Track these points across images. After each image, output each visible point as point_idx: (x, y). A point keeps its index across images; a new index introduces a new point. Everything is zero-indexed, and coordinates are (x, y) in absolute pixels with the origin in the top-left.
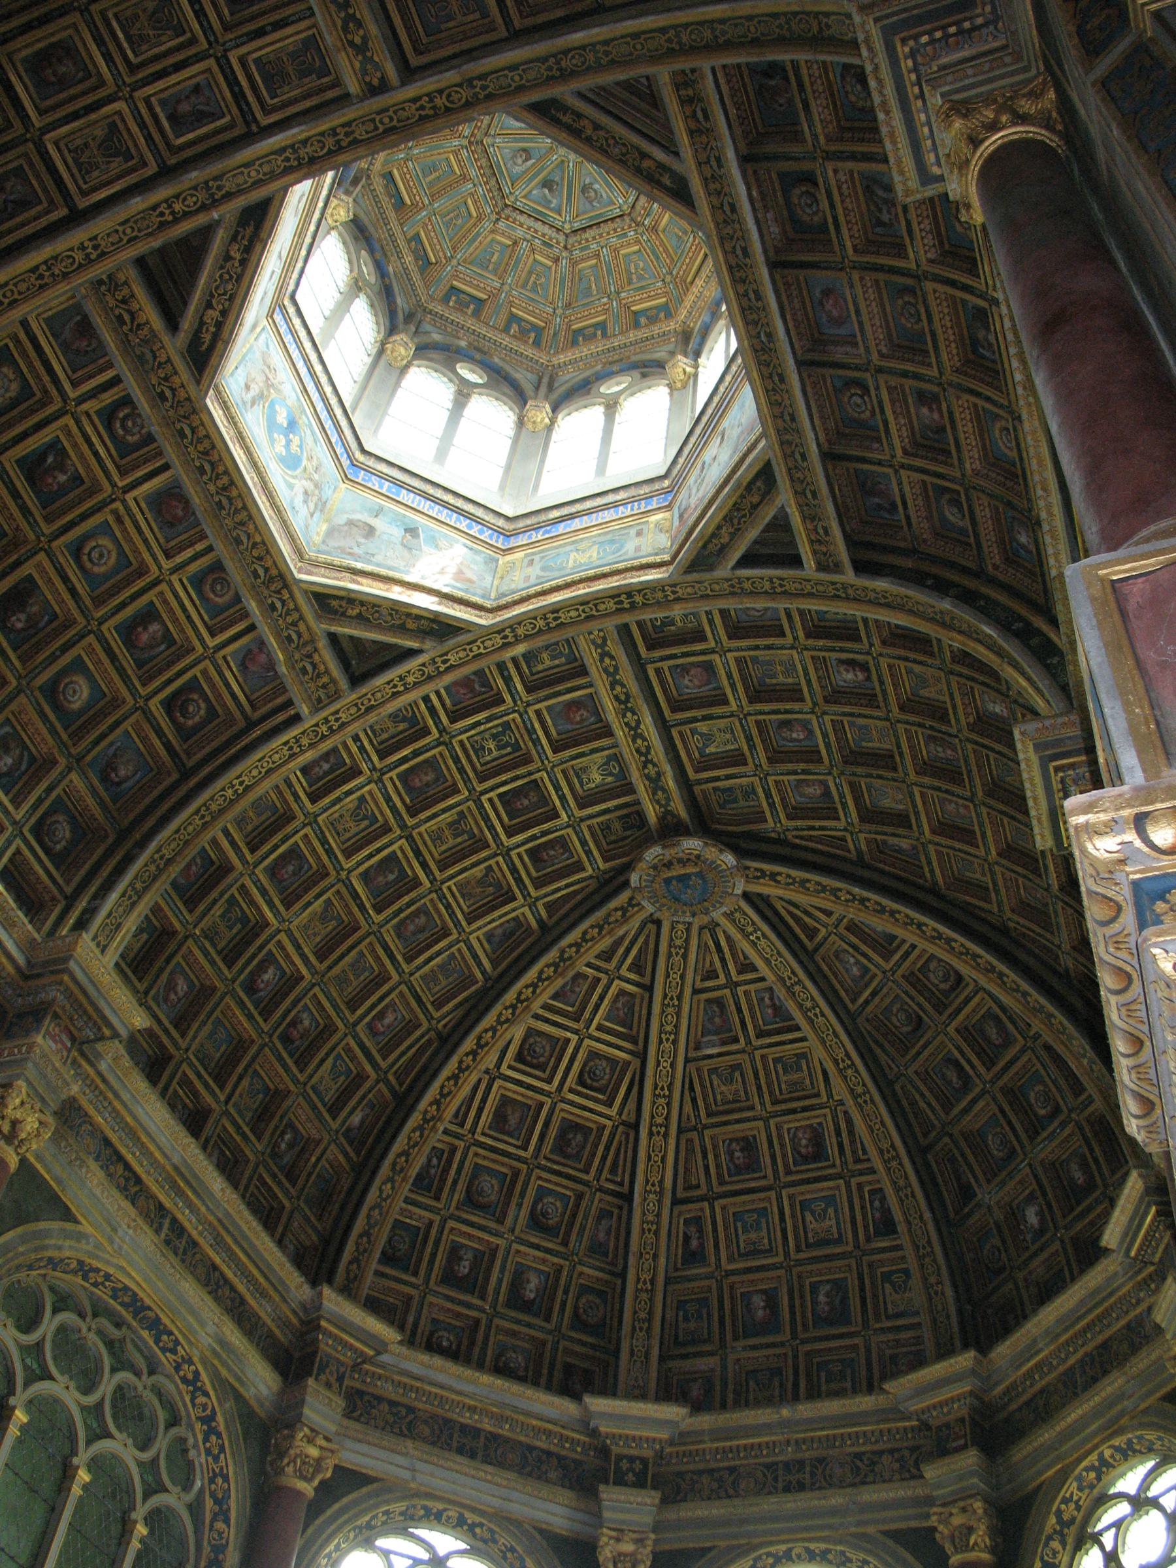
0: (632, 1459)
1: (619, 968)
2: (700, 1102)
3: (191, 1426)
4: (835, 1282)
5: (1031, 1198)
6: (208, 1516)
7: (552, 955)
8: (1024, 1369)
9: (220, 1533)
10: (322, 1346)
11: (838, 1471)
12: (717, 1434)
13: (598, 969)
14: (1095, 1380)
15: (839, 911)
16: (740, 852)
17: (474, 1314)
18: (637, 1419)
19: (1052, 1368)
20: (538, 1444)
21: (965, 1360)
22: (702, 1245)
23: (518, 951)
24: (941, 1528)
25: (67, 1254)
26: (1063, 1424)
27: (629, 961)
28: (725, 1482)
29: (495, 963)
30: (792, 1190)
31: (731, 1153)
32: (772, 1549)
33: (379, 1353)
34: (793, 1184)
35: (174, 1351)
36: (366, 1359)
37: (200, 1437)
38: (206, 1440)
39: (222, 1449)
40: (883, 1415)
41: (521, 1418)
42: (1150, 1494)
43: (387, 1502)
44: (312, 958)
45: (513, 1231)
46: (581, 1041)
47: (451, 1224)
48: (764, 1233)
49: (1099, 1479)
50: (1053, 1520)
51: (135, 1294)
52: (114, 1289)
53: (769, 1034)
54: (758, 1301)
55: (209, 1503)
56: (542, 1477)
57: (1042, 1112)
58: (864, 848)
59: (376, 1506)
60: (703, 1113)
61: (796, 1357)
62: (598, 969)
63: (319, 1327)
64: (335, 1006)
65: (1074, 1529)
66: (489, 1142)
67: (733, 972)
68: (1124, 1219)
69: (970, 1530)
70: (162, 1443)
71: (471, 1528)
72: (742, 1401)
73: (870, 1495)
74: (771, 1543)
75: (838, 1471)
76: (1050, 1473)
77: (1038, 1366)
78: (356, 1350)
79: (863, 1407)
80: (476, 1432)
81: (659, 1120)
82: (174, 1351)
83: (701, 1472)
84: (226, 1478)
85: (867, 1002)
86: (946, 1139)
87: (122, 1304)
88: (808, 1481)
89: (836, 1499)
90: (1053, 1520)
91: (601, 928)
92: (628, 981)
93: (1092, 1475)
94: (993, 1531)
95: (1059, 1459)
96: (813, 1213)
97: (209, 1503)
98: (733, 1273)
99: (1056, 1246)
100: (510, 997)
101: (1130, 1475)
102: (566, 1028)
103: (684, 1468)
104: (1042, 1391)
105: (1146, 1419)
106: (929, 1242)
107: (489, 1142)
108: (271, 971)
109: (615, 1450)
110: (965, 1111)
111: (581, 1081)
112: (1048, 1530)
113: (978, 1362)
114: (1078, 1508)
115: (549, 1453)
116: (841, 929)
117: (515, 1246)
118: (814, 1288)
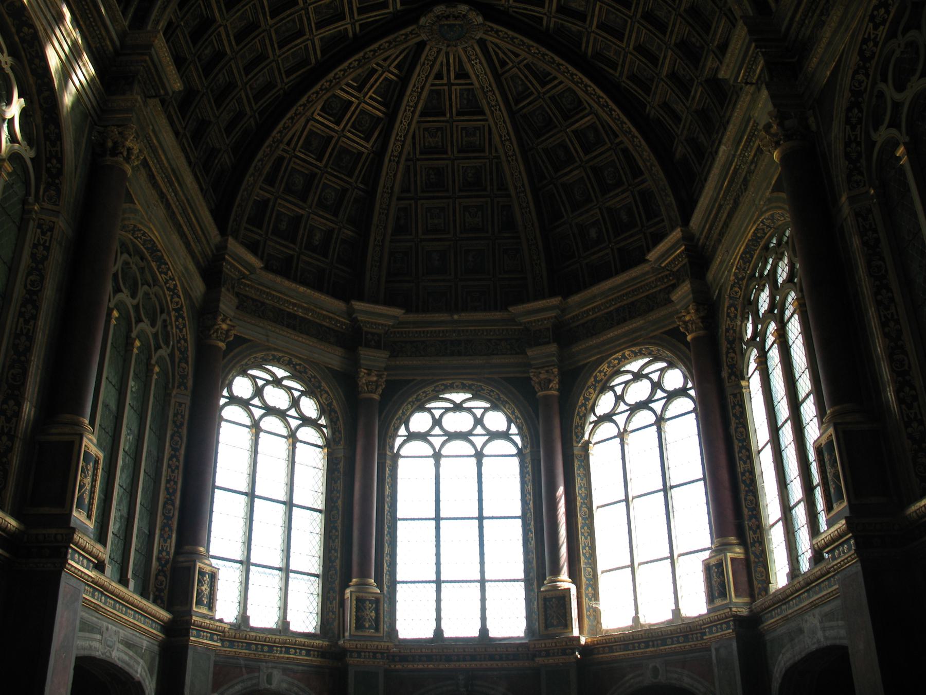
1: (389, 66)
3: (169, 314)
6: (177, 360)
9: (184, 369)
14: (625, 320)
15: (523, 54)
16: (486, 18)
18: (376, 314)
20: (324, 323)
21: (555, 301)
24: (534, 379)
26: (605, 337)
27: (396, 62)
32: (445, 382)
33: (251, 273)
35: (166, 274)
36: (244, 276)
37: (173, 319)
38: (177, 320)
39: (185, 326)
42: (644, 372)
45: (310, 207)
46: (359, 104)
47: (279, 201)
49: (619, 363)
50: (592, 379)
55: (177, 353)
58: (552, 25)
59: (250, 355)
63: (224, 259)
65: (601, 384)
66: (303, 156)
68: (664, 249)
69: (550, 381)
71: (294, 366)
73: (496, 360)
76: (594, 358)
77: (593, 308)
78: (239, 271)
80: (295, 316)
81: (395, 153)
82: (166, 274)
84: (186, 341)
85: (524, 107)
90: (592, 379)
92: (392, 73)
93: (616, 361)
94: (561, 382)
95: (598, 353)
97: (177, 353)
101: (634, 363)
105: (653, 341)
107: (303, 156)
109: (365, 329)
110: (566, 174)
111: (353, 126)
112: (589, 383)
114: (605, 375)
116: (521, 66)
117: (312, 216)
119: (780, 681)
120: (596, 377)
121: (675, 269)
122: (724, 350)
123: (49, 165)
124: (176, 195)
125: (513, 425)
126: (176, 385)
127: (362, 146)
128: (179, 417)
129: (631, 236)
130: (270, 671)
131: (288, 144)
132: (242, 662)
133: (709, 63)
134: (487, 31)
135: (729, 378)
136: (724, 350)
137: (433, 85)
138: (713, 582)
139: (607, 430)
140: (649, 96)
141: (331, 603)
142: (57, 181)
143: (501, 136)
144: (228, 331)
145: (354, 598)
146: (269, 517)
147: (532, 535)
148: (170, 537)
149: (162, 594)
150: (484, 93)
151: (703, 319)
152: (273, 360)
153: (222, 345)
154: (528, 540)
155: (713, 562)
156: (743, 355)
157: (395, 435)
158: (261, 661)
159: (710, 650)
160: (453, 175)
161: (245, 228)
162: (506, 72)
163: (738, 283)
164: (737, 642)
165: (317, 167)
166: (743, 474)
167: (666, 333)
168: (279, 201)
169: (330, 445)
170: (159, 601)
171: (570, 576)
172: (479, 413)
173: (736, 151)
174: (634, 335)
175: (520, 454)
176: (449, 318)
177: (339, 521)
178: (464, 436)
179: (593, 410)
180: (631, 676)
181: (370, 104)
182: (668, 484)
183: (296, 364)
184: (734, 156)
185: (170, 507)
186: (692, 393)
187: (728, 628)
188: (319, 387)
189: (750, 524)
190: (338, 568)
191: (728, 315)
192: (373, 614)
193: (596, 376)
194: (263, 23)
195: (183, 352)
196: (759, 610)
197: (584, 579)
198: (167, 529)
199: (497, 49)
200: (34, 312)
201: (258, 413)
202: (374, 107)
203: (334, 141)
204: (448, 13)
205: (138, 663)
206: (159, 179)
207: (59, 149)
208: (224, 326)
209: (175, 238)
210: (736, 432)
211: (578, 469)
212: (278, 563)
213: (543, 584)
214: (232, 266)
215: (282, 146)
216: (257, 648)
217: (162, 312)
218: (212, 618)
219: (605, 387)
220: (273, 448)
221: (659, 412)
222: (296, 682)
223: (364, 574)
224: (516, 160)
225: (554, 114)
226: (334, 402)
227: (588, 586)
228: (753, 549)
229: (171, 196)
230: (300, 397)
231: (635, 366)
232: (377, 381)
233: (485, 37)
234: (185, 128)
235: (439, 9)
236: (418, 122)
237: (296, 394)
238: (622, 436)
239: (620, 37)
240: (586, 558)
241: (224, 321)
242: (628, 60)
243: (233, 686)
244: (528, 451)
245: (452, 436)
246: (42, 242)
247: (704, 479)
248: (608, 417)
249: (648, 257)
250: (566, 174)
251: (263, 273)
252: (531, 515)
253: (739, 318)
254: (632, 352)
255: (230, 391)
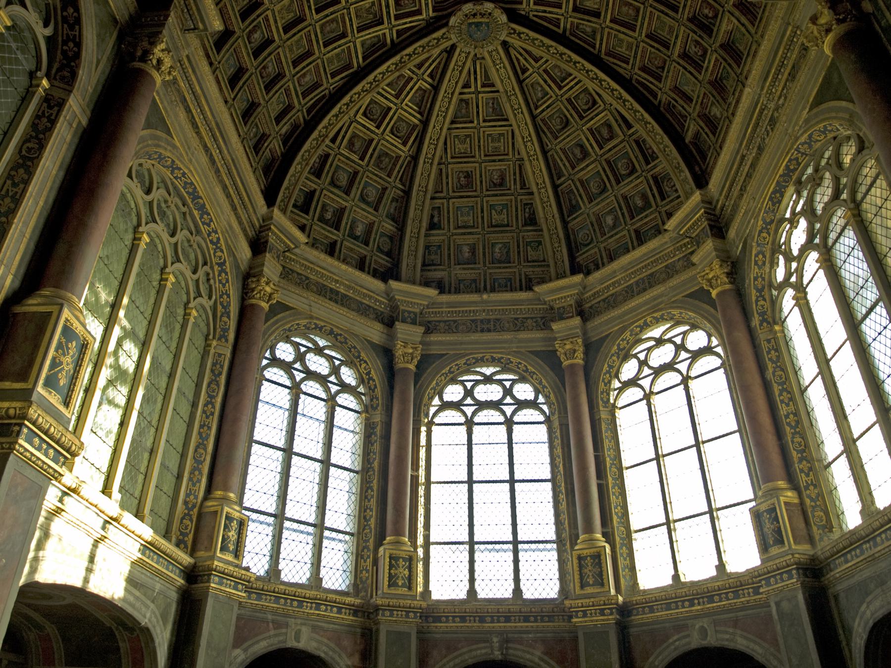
0: (409, 312)
2: (449, 151)
3: (212, 268)
4: (504, 244)
5: (610, 212)
6: (219, 314)
7: (397, 58)
8: (606, 284)
9: (226, 323)
10: (270, 239)
11: (507, 325)
12: (450, 305)
13: (413, 72)
14: (645, 290)
17: (335, 238)
18: (411, 294)
19: (620, 284)
22: (440, 221)
23: (379, 53)
24: (560, 349)
25: (169, 154)
28: (451, 327)
29: (364, 59)
30: (488, 198)
31: (459, 178)
33: (296, 247)
34: (489, 196)
35: (209, 225)
37: (216, 274)
38: (219, 275)
39: (227, 281)
40: (529, 301)
41: (359, 288)
42: (666, 338)
43: (299, 319)
44: (281, 31)
46: (397, 110)
48: (471, 218)
49: (641, 331)
51: (195, 188)
52: (186, 183)
53: (490, 121)
54: (466, 249)
56: (367, 316)
57: (624, 172)
58: (568, 26)
59: (293, 321)
60: (449, 156)
61: (485, 275)
62: (413, 72)
64: (287, 62)
67: (479, 86)
69: (575, 351)
70: (201, 273)
71: (336, 336)
72: (458, 291)
73: (523, 335)
74: (475, 353)
75: (507, 325)
77: (614, 283)
79: (522, 297)
80: (337, 293)
81: (430, 156)
82: (209, 225)
83: (439, 322)
84: (228, 296)
86: (570, 181)
87: (187, 193)
88: (492, 328)
89: (507, 336)
91: (424, 48)
92: (426, 82)
96: (496, 211)
97: (219, 307)
98: (456, 234)
99: (625, 232)
100: (371, 78)
102: (392, 102)
103: (430, 319)
104: (612, 295)
106: (556, 228)
108: (258, 33)
109: (402, 308)
112: (613, 352)
113: (583, 280)
114: (628, 343)
115: (370, 307)
116: (541, 71)
117: (354, 208)
118: (493, 245)
119: (865, 637)
120: (619, 345)
121: (693, 235)
122: (754, 298)
123: (65, 48)
124: (220, 152)
125: (540, 396)
126: (217, 337)
127: (400, 149)
128: (218, 366)
129: (646, 216)
130: (299, 627)
131: (333, 141)
132: (270, 617)
133: (724, 27)
134: (510, 33)
135: (761, 325)
136: (754, 298)
137: (461, 94)
138: (766, 530)
139: (633, 393)
140: (660, 82)
141: (365, 561)
142: (73, 64)
143: (523, 138)
144: (271, 295)
145: (387, 555)
146: (304, 475)
147: (562, 497)
148: (199, 481)
149: (186, 539)
150: (508, 97)
151: (728, 275)
152: (315, 328)
153: (265, 305)
154: (559, 502)
155: (763, 507)
156: (775, 304)
157: (429, 405)
158: (290, 616)
159: (770, 606)
160: (481, 176)
161: (292, 211)
162: (527, 78)
163: (766, 228)
164: (804, 594)
165: (359, 165)
166: (787, 416)
167: (689, 296)
168: (325, 192)
169: (366, 410)
170: (182, 546)
171: (604, 535)
172: (508, 384)
173: (762, 89)
174: (655, 302)
175: (548, 421)
176: (479, 299)
177: (375, 482)
178: (495, 405)
179: (617, 376)
180: (675, 638)
181: (407, 111)
182: (700, 440)
183: (338, 335)
184: (760, 95)
185: (202, 451)
186: (719, 350)
187: (790, 577)
188: (359, 357)
189: (801, 466)
190: (373, 526)
191: (756, 263)
192: (406, 572)
193: (619, 345)
194: (317, 51)
195: (226, 307)
196: (828, 554)
197: (617, 539)
198: (197, 473)
199: (518, 56)
200: (26, 177)
201: (299, 376)
202: (410, 114)
203: (374, 143)
204: (475, 11)
205: (147, 607)
206: (202, 130)
207: (77, 33)
208: (268, 289)
209: (218, 190)
210: (774, 376)
211: (606, 432)
212: (281, 444)
213: (576, 544)
214: (278, 237)
215: (327, 141)
216: (286, 603)
217: (205, 264)
218: (238, 566)
219: (626, 357)
220: (313, 408)
221: (685, 373)
222: (326, 641)
223: (398, 532)
224: (537, 159)
225: (571, 115)
226: (373, 372)
227: (622, 545)
228: (808, 492)
229: (215, 153)
230: (340, 366)
231: (656, 332)
232: (412, 354)
233: (508, 39)
234: (234, 100)
235: (468, 8)
236: (449, 129)
237: (337, 363)
238: (648, 397)
239: (632, 28)
240: (618, 517)
241: (267, 284)
242: (640, 49)
243: (257, 642)
244: (556, 416)
245: (482, 405)
246: (47, 115)
247: (739, 431)
248: (633, 382)
249: (666, 227)
250: (583, 169)
251: (308, 249)
252: (561, 478)
253: (768, 265)
254: (654, 317)
255: (273, 353)
